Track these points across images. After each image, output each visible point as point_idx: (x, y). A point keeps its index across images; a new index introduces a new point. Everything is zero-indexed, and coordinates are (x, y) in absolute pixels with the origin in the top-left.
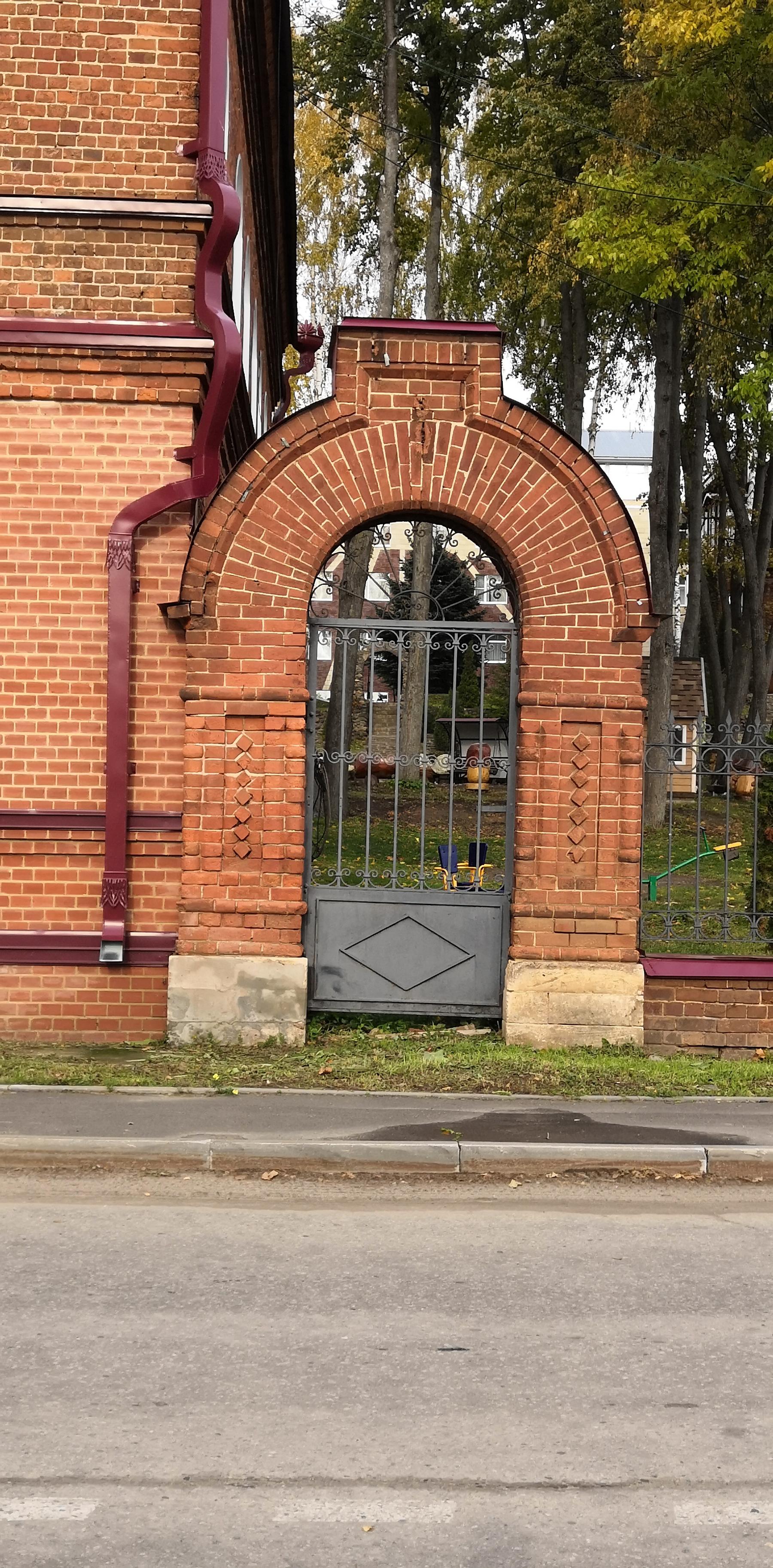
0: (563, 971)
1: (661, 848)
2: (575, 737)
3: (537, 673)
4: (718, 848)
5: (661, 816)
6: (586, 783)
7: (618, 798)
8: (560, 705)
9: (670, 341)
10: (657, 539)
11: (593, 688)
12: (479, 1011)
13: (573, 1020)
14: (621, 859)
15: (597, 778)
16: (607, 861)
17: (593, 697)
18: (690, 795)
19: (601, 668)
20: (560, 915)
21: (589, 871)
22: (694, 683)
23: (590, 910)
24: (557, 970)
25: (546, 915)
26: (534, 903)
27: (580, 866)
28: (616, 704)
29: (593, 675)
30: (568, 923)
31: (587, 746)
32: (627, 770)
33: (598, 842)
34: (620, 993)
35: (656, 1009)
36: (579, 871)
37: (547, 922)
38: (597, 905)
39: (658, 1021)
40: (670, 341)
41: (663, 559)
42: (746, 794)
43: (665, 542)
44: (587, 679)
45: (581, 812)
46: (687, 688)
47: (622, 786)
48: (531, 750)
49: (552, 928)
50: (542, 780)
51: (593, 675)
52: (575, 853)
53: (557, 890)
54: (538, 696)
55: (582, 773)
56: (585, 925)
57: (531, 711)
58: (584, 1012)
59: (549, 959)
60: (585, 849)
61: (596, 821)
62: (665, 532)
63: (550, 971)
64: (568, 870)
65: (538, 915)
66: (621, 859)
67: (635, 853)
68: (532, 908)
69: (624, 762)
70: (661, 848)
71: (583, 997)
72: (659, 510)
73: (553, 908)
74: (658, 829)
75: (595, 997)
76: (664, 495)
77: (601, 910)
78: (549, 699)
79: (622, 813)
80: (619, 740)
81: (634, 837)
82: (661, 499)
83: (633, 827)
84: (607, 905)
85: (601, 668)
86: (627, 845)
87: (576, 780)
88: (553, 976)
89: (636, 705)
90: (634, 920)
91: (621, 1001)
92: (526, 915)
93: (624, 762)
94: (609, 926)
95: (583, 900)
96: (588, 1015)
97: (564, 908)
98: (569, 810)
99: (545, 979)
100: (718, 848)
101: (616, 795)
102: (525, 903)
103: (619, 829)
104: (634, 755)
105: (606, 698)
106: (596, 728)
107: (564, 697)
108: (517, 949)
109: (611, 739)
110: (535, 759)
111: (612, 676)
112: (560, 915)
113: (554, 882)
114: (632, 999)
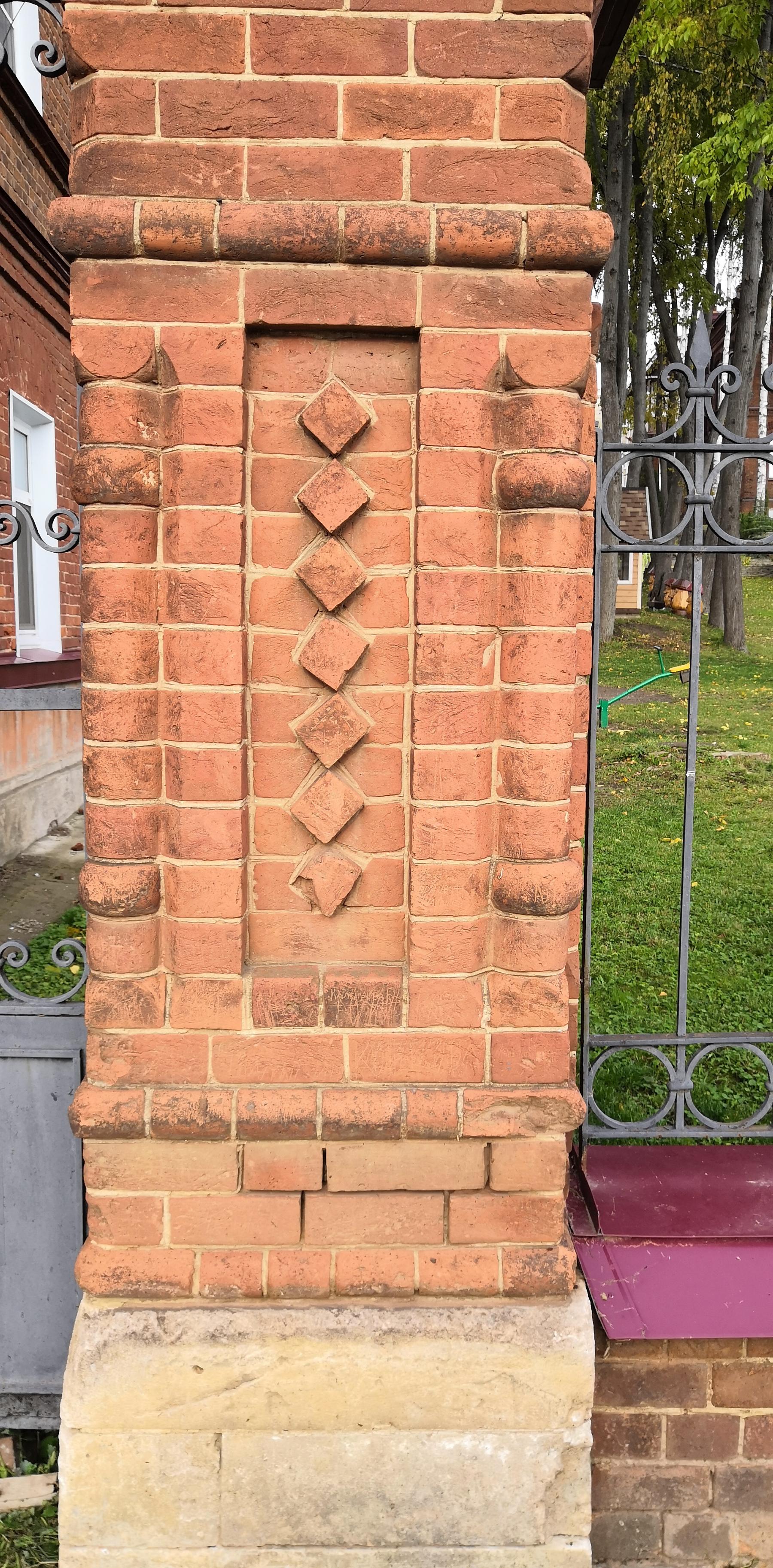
0: (273, 1350)
1: (611, 661)
2: (310, 398)
3: (133, 110)
4: (674, 669)
5: (610, 631)
6: (359, 593)
7: (492, 654)
8: (238, 252)
9: (620, 180)
10: (607, 374)
11: (380, 176)
12: (20, 1406)
13: (314, 1528)
14: (506, 903)
15: (404, 570)
16: (449, 912)
17: (377, 215)
18: (635, 611)
19: (412, 79)
20: (256, 1130)
21: (383, 948)
22: (639, 510)
23: (380, 1110)
24: (252, 1350)
25: (211, 1130)
26: (159, 1084)
27: (346, 926)
28: (474, 239)
29: (376, 113)
30: (297, 1157)
31: (360, 435)
32: (529, 532)
33: (403, 829)
34: (499, 1426)
35: (639, 1438)
36: (340, 950)
37: (215, 1157)
38: (411, 1084)
39: (645, 1483)
40: (620, 180)
41: (612, 393)
42: (681, 609)
43: (615, 378)
44: (354, 129)
45: (338, 714)
46: (634, 514)
47: (509, 603)
48: (118, 457)
49: (231, 1175)
50: (174, 583)
51: (376, 113)
52: (321, 882)
53: (248, 1031)
54: (135, 212)
55: (337, 554)
56: (354, 1161)
57: (110, 284)
58: (358, 1502)
59: (224, 1297)
60: (363, 861)
61: (405, 747)
62: (614, 367)
63: (220, 1352)
64: (300, 944)
65: (165, 1131)
66: (506, 903)
67: (561, 878)
68: (148, 1105)
69: (517, 499)
70: (611, 661)
71: (355, 1447)
72: (609, 347)
73: (229, 1108)
74: (608, 643)
75: (402, 1444)
76: (613, 332)
77: (423, 1109)
78: (187, 225)
79: (507, 714)
80: (496, 406)
81: (555, 810)
82: (611, 336)
83: (556, 775)
84: (450, 1086)
85: (412, 79)
86: (529, 844)
87: (318, 582)
88: (236, 1371)
89: (562, 245)
90: (556, 1139)
91: (504, 1455)
92: (129, 1132)
93: (517, 499)
94: (459, 1163)
95: (353, 1073)
96: (374, 1509)
97: (272, 1105)
98: (300, 706)
99: (202, 1382)
100: (674, 669)
101: (481, 645)
102: (121, 1084)
103: (497, 780)
104: (559, 469)
105: (431, 221)
106: (391, 361)
107: (248, 214)
108: (102, 1255)
109: (464, 403)
110: (139, 496)
111: (460, 115)
112: (256, 1130)
113: (234, 999)
114: (547, 1446)
